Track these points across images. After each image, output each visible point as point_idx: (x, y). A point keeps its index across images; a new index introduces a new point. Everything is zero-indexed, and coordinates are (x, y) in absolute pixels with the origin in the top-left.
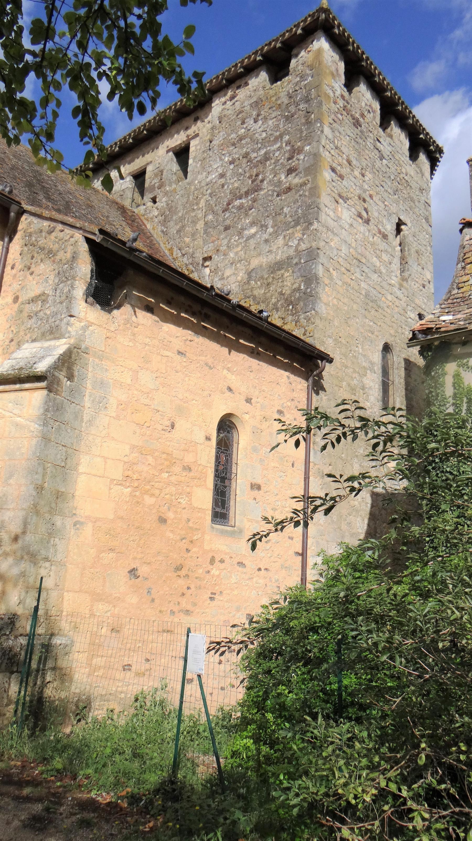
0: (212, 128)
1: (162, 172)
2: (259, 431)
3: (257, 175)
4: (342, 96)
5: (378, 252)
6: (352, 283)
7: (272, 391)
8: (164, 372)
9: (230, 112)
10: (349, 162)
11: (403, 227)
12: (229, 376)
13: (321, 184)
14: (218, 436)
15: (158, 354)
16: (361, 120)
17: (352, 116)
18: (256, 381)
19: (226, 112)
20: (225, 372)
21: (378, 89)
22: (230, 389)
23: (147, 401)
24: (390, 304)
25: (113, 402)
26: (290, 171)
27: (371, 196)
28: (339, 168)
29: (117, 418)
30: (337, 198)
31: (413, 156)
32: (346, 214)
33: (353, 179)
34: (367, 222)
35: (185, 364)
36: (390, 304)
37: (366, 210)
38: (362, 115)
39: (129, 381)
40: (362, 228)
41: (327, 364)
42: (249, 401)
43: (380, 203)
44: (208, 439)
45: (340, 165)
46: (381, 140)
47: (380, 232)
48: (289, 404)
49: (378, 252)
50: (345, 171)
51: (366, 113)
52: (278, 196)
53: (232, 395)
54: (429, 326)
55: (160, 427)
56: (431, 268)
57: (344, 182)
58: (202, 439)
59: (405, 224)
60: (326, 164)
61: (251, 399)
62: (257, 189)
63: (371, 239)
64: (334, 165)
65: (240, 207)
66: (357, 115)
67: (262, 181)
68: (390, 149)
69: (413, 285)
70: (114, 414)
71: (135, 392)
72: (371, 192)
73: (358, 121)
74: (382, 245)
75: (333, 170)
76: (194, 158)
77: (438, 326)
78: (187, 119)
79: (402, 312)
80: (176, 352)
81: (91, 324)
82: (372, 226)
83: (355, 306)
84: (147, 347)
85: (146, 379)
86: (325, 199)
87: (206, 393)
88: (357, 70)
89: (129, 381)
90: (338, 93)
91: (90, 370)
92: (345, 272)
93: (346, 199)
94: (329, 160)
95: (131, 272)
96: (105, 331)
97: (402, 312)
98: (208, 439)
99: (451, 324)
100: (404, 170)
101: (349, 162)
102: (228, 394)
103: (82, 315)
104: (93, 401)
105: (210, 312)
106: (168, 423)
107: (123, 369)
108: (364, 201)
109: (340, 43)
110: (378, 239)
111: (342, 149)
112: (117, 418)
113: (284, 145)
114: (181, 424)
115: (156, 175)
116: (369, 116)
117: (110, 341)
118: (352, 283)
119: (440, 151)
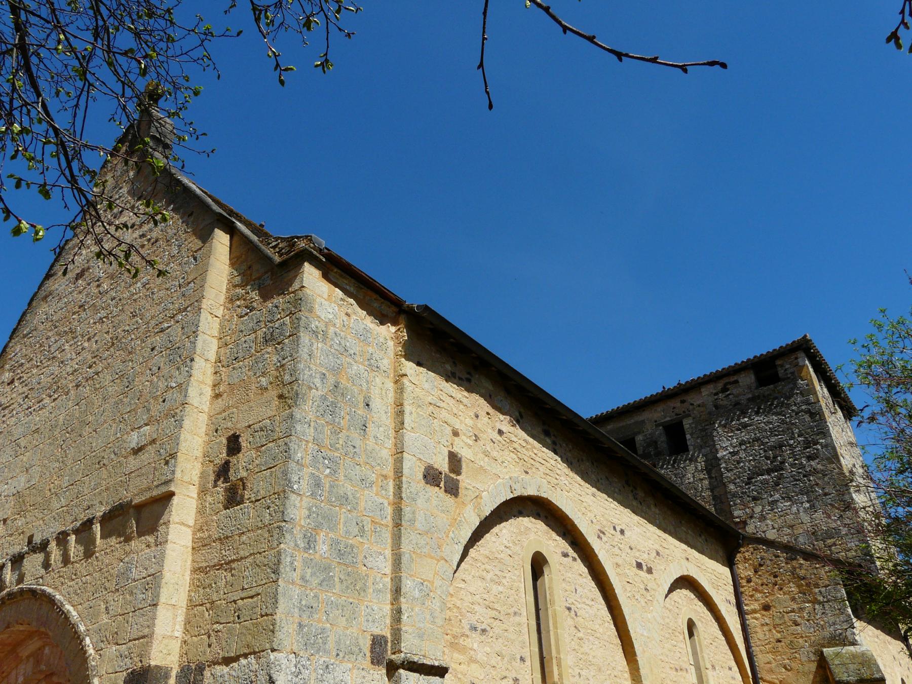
26: (809, 458)
65: (765, 482)
76: (691, 434)
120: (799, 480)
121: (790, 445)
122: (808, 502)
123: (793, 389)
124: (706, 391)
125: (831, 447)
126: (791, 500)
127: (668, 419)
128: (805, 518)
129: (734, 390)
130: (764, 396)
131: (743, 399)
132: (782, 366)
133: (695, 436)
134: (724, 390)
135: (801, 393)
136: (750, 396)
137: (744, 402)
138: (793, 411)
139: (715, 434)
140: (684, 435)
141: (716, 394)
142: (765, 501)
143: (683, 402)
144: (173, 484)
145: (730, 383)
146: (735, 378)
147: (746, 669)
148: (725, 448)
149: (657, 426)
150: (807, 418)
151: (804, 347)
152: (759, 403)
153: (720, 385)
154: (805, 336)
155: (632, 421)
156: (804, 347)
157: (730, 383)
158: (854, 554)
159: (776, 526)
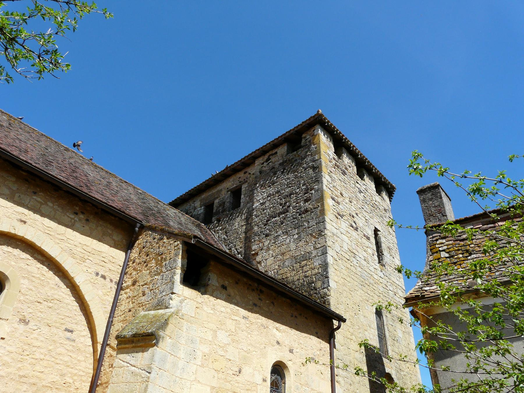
0: (256, 177)
1: (224, 203)
2: (299, 374)
3: (285, 203)
4: (334, 158)
5: (364, 247)
6: (352, 268)
7: (295, 345)
8: (234, 331)
9: (266, 168)
10: (341, 194)
11: (378, 233)
12: (277, 333)
13: (326, 207)
14: (271, 378)
15: (230, 318)
16: (346, 171)
17: (340, 169)
18: (295, 336)
19: (264, 169)
20: (275, 330)
21: (354, 155)
22: (278, 343)
23: (222, 353)
24: (377, 281)
25: (199, 354)
26: (306, 201)
27: (357, 214)
28: (336, 198)
29: (202, 366)
30: (337, 215)
31: (379, 192)
32: (344, 225)
33: (345, 204)
34: (356, 229)
35: (248, 325)
36: (377, 281)
37: (354, 222)
38: (346, 169)
39: (210, 339)
40: (354, 233)
41: (342, 323)
42: (291, 351)
43: (362, 218)
44: (264, 380)
45: (336, 196)
46: (358, 182)
47: (365, 236)
48: (318, 353)
49: (364, 247)
50: (340, 200)
51: (348, 167)
52: (299, 215)
53: (280, 347)
54: (417, 294)
55: (231, 372)
56: (398, 257)
57: (340, 206)
58: (260, 381)
59: (379, 231)
60: (328, 195)
61: (293, 350)
62: (286, 211)
63: (360, 240)
64: (334, 196)
65: (275, 223)
66: (344, 168)
67: (289, 207)
68: (364, 187)
69: (388, 269)
70: (200, 363)
71: (215, 346)
72: (357, 212)
73: (344, 171)
74: (367, 243)
75: (333, 199)
76: (244, 195)
77: (423, 294)
78: (240, 173)
79: (385, 286)
80: (242, 317)
81: (186, 298)
82: (359, 232)
83: (356, 283)
84: (223, 314)
85: (223, 337)
86: (329, 217)
87: (263, 346)
88: (341, 145)
89: (210, 339)
90: (331, 157)
91: (184, 331)
92: (347, 261)
93: (342, 216)
94: (330, 193)
95: (212, 263)
96: (195, 303)
97: (385, 286)
98: (264, 380)
99: (431, 292)
100: (374, 199)
101: (341, 194)
102: (277, 346)
103: (180, 293)
104: (185, 353)
105: (264, 289)
106: (237, 369)
107: (206, 330)
108: (353, 217)
109: (331, 132)
110: (364, 240)
111: (337, 187)
112: (202, 366)
113: (301, 185)
114: (246, 370)
115: (220, 205)
116: (350, 170)
117: (198, 310)
118: (352, 268)
119: (393, 188)
120: (296, 218)
121: (296, 193)
122: (297, 234)
123: (307, 152)
124: (258, 162)
125: (321, 191)
126: (287, 234)
127: (235, 186)
128: (293, 246)
129: (273, 159)
130: (289, 160)
131: (277, 165)
132: (305, 137)
133: (246, 195)
134: (268, 159)
135: (311, 155)
136: (281, 161)
137: (277, 166)
138: (303, 168)
139: (255, 191)
140: (241, 195)
141: (263, 164)
142: (272, 237)
143: (245, 173)
144: (370, 342)
145: (272, 155)
146: (276, 150)
147: (97, 351)
148: (258, 201)
149: (228, 192)
150: (311, 171)
151: (439, 185)
152: (287, 165)
153: (266, 157)
154: (318, 111)
155: (216, 190)
156: (318, 121)
157: (272, 155)
158: (317, 271)
159: (274, 254)
